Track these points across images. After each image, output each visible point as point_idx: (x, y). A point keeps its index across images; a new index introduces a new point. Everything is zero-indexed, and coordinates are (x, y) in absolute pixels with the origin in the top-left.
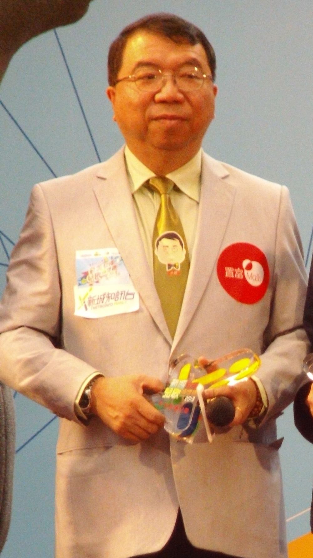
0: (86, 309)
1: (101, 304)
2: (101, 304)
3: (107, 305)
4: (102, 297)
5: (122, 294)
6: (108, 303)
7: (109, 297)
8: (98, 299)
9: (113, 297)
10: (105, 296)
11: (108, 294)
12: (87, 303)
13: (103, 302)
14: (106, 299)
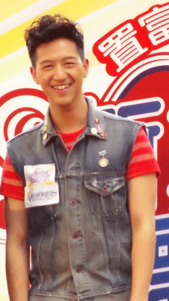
0: (30, 201)
1: (38, 198)
2: (38, 198)
3: (41, 199)
4: (38, 194)
5: (50, 193)
6: (41, 198)
7: (42, 195)
8: (36, 195)
9: (44, 195)
11: (42, 193)
12: (30, 197)
13: (38, 197)
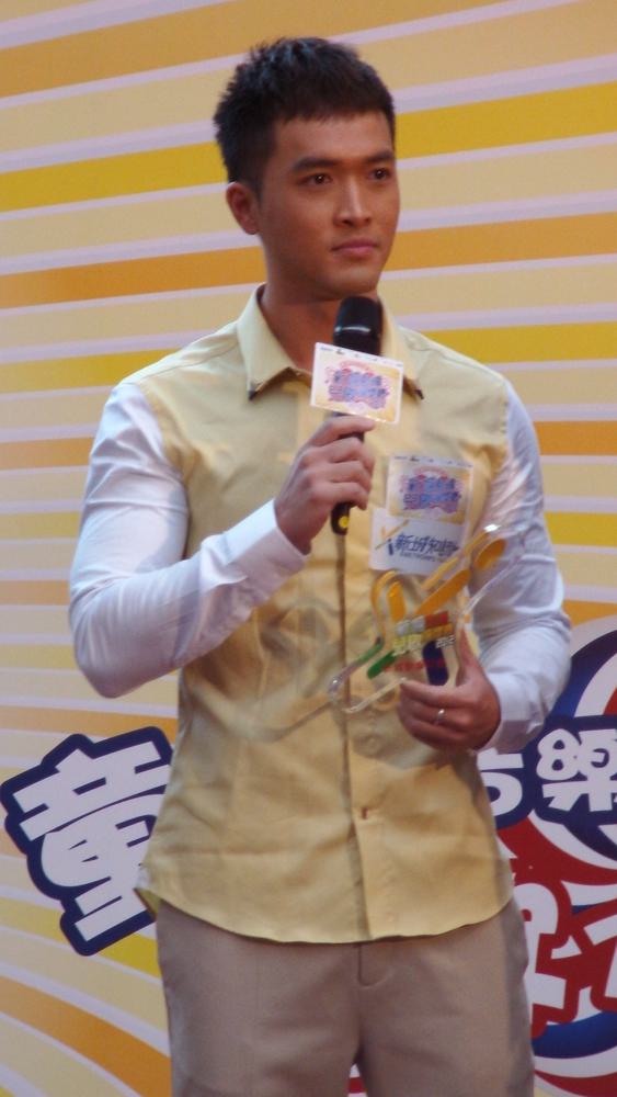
7: (432, 546)
10: (428, 542)
14: (427, 548)
